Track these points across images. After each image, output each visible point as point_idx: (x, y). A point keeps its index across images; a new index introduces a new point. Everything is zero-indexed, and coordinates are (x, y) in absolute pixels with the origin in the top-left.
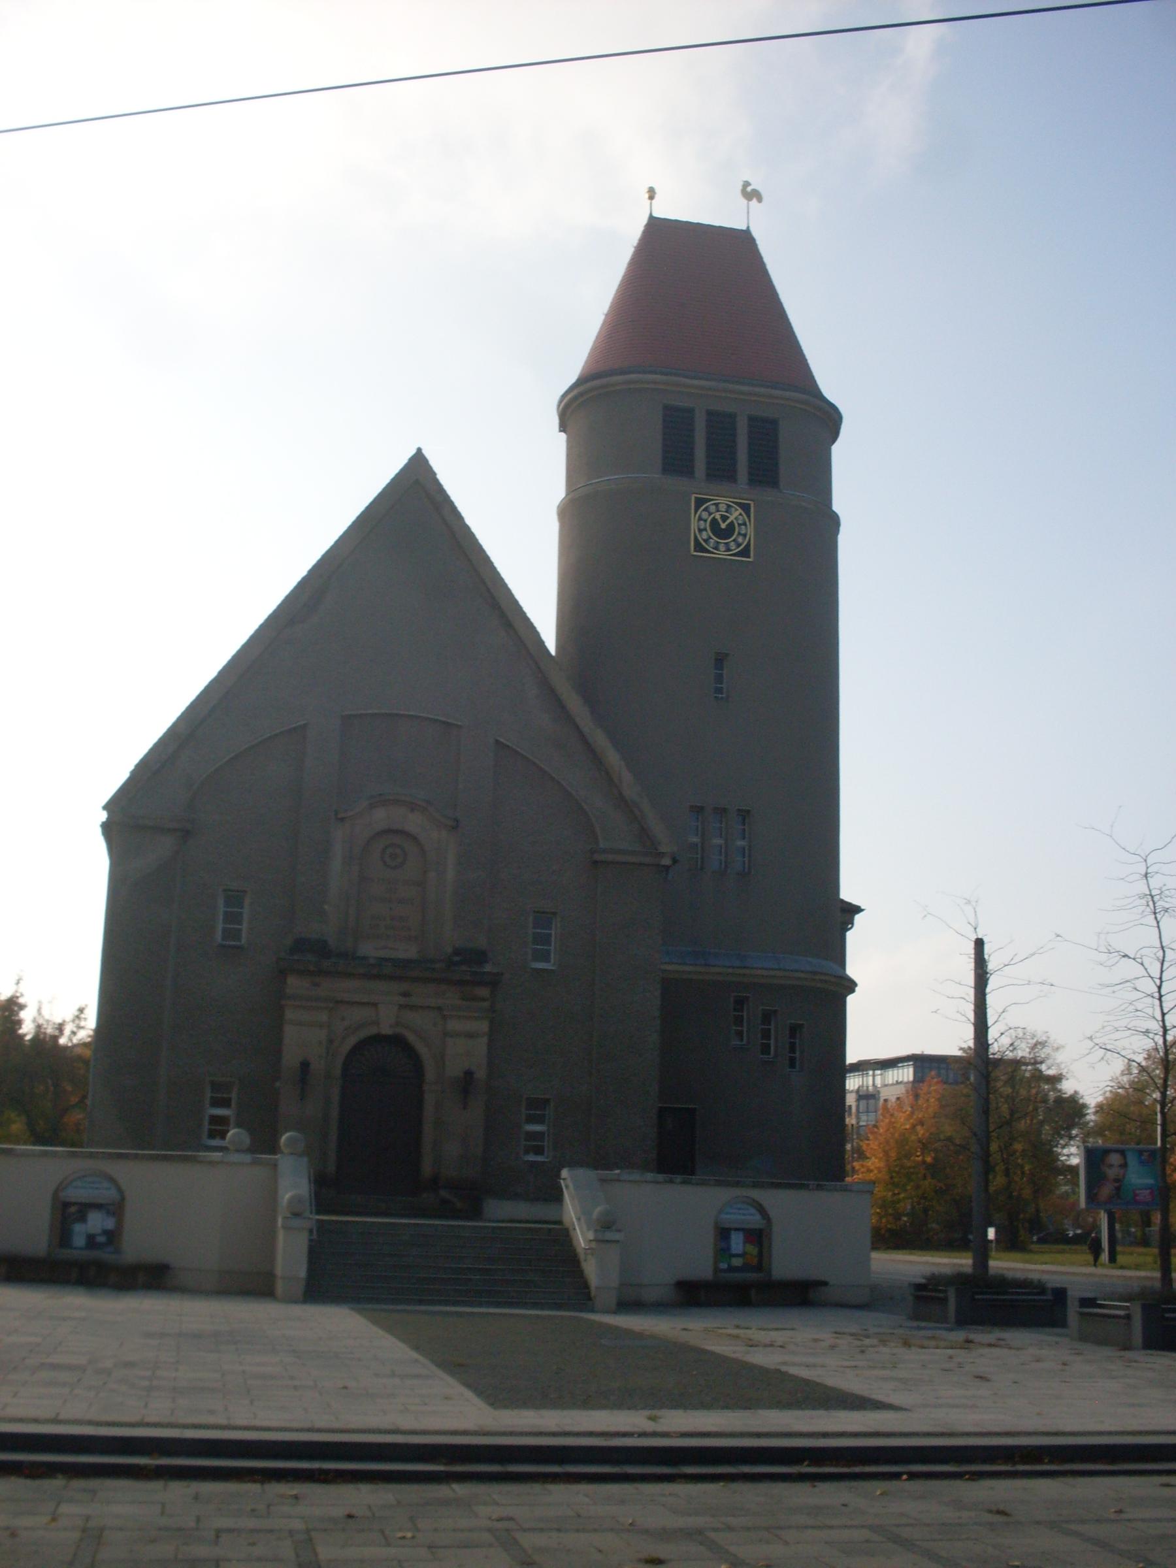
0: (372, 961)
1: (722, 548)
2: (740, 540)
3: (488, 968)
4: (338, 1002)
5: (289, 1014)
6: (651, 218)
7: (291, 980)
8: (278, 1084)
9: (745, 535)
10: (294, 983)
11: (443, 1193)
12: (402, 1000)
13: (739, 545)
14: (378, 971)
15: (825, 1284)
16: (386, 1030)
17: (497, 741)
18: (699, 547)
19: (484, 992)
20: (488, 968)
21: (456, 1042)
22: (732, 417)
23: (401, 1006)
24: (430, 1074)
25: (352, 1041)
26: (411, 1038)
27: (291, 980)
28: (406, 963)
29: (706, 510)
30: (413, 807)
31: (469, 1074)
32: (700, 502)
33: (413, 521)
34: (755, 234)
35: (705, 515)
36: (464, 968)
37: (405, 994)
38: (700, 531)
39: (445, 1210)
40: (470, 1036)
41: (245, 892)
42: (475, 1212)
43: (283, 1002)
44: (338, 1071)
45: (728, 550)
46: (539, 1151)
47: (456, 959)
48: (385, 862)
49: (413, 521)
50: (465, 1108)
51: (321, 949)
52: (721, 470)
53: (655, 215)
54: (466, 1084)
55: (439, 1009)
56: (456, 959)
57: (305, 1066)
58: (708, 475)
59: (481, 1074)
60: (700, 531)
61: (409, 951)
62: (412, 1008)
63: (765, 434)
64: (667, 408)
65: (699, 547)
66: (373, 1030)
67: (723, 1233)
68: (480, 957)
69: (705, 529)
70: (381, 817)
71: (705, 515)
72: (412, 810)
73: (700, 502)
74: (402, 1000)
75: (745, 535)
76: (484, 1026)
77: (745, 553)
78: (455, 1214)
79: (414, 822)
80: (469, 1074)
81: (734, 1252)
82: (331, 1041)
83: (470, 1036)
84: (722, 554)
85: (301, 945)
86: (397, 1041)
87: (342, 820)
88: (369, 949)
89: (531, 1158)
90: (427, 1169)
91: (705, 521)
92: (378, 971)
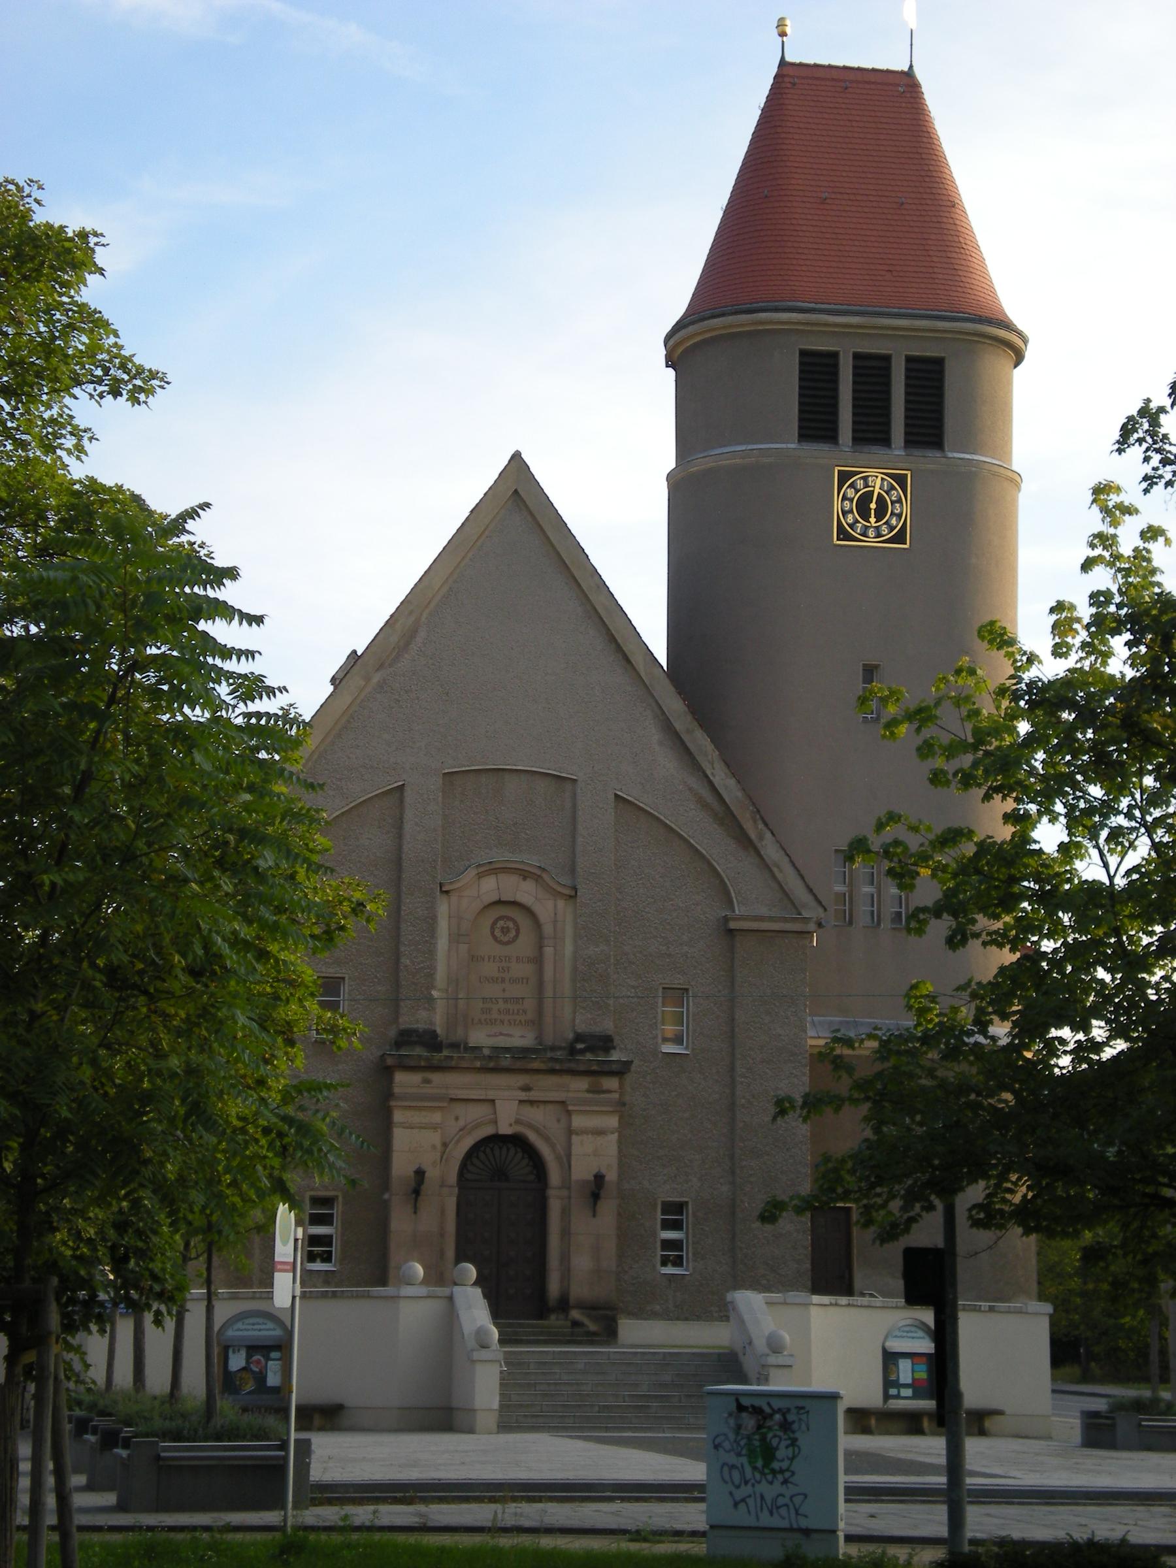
0: (486, 1052)
1: (871, 533)
2: (894, 521)
3: (615, 1056)
4: (452, 1099)
5: (398, 1116)
6: (783, 63)
7: (400, 1077)
8: (386, 1196)
9: (899, 516)
10: (403, 1080)
11: (575, 1314)
12: (523, 1095)
13: (892, 528)
14: (496, 1062)
15: (1000, 1413)
16: (505, 1129)
17: (616, 795)
18: (843, 534)
19: (612, 1083)
20: (615, 1056)
21: (587, 1142)
22: (311, 1214)
23: (520, 1101)
24: (554, 1176)
25: (468, 1142)
26: (532, 1137)
27: (400, 1077)
28: (522, 1053)
29: (852, 486)
30: (525, 875)
31: (599, 1178)
32: (844, 477)
33: (517, 521)
34: (920, 75)
35: (850, 493)
36: (589, 1056)
37: (526, 1088)
38: (844, 513)
39: (577, 1334)
40: (600, 1132)
41: (343, 978)
42: (610, 1333)
43: (393, 1103)
44: (453, 1178)
45: (879, 535)
46: (678, 1261)
47: (580, 1046)
48: (493, 934)
49: (517, 521)
50: (594, 1216)
51: (431, 1041)
52: (871, 432)
53: (789, 58)
54: (596, 1188)
55: (563, 1103)
56: (580, 1046)
57: (420, 1174)
58: (855, 439)
59: (611, 1176)
60: (844, 513)
61: (521, 1038)
62: (532, 1103)
63: (928, 378)
64: (803, 353)
65: (843, 534)
66: (488, 1131)
67: (890, 1358)
68: (605, 1043)
69: (851, 511)
70: (490, 887)
71: (850, 493)
72: (525, 878)
73: (844, 477)
74: (523, 1095)
75: (899, 516)
76: (613, 1121)
77: (899, 538)
78: (591, 1338)
79: (526, 892)
80: (599, 1178)
81: (902, 1381)
82: (445, 1145)
83: (600, 1132)
84: (871, 541)
85: (406, 1038)
86: (518, 1142)
87: (447, 892)
88: (479, 1037)
89: (670, 1270)
90: (554, 1287)
91: (851, 500)
92: (496, 1062)
